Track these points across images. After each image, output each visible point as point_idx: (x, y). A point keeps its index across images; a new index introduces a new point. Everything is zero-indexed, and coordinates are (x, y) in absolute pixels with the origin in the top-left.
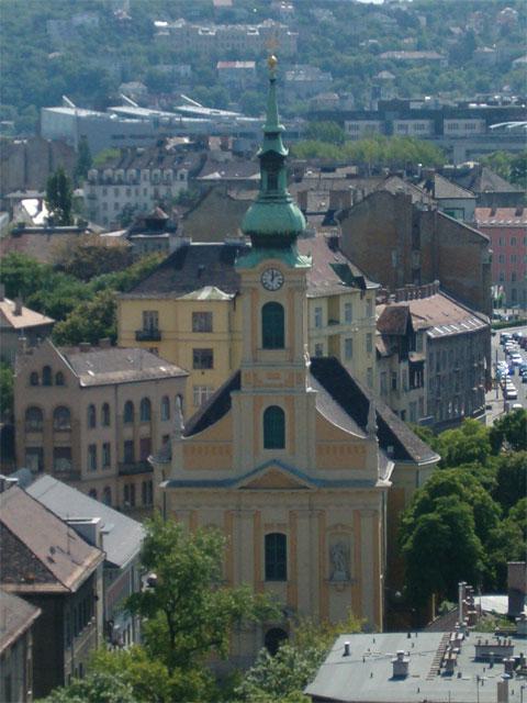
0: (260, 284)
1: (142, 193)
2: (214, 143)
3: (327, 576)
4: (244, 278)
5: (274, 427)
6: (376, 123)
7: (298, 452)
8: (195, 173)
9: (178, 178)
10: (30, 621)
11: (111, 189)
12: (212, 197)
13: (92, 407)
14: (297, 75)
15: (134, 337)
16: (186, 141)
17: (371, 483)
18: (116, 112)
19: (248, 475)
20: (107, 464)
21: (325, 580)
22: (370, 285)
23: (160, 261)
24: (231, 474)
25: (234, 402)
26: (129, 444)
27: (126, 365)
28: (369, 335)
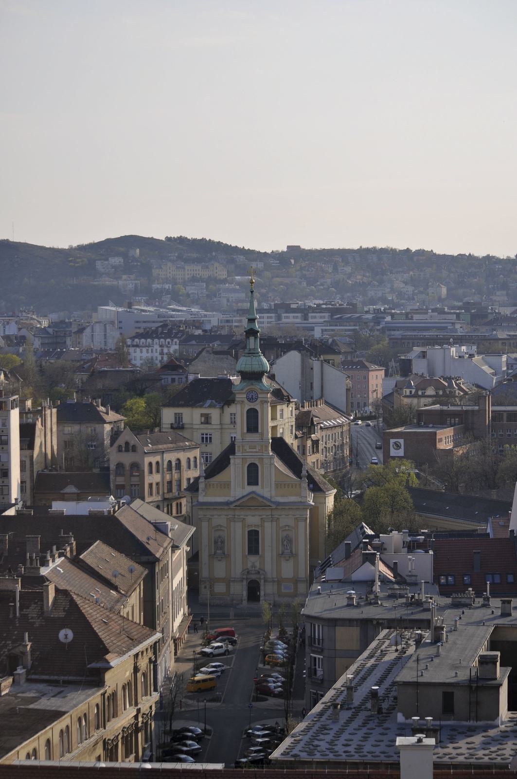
0: (246, 399)
1: (154, 351)
3: (281, 553)
4: (237, 396)
6: (273, 315)
7: (265, 489)
9: (174, 343)
11: (138, 350)
15: (170, 426)
18: (137, 309)
19: (239, 499)
21: (279, 554)
24: (232, 499)
25: (232, 461)
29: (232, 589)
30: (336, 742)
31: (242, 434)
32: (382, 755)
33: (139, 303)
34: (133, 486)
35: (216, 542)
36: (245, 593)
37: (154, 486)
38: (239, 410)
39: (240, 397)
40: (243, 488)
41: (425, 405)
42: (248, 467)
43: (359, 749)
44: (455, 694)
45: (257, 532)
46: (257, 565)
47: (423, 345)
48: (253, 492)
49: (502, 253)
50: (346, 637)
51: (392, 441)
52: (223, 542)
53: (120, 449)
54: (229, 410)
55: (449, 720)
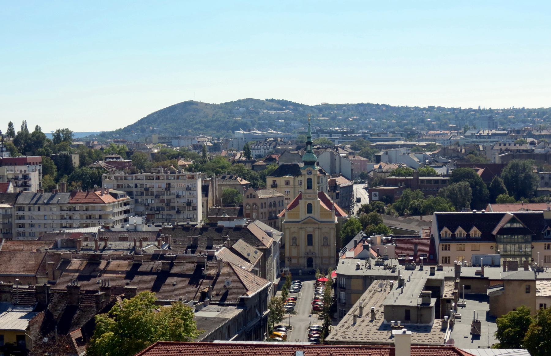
2: (279, 140)
5: (310, 208)
6: (316, 135)
7: (315, 214)
8: (274, 147)
10: (261, 255)
12: (286, 153)
13: (262, 204)
14: (294, 123)
16: (272, 139)
17: (334, 222)
20: (265, 218)
22: (327, 174)
23: (6, 167)
26: (271, 212)
27: (270, 193)
28: (327, 186)
29: (300, 261)
30: (355, 333)
31: (305, 190)
32: (377, 339)
33: (254, 130)
34: (84, 209)
35: (292, 240)
36: (306, 263)
37: (264, 214)
38: (303, 179)
39: (303, 172)
40: (305, 214)
41: (388, 177)
42: (308, 205)
43: (366, 336)
44: (411, 312)
45: (311, 235)
46: (312, 250)
47: (386, 149)
48: (310, 217)
49: (546, 107)
50: (356, 285)
51: (373, 193)
52: (296, 240)
53: (248, 197)
54: (299, 178)
55: (408, 323)
